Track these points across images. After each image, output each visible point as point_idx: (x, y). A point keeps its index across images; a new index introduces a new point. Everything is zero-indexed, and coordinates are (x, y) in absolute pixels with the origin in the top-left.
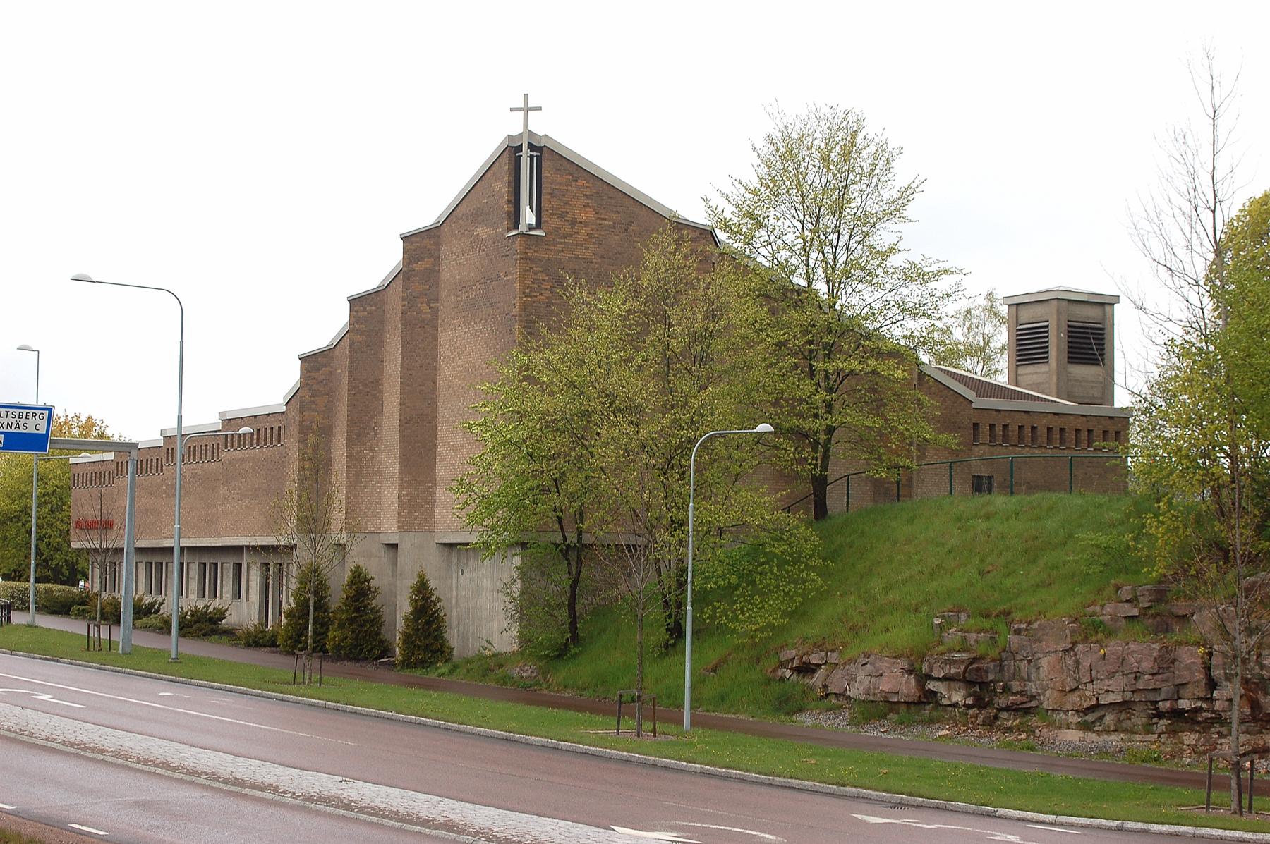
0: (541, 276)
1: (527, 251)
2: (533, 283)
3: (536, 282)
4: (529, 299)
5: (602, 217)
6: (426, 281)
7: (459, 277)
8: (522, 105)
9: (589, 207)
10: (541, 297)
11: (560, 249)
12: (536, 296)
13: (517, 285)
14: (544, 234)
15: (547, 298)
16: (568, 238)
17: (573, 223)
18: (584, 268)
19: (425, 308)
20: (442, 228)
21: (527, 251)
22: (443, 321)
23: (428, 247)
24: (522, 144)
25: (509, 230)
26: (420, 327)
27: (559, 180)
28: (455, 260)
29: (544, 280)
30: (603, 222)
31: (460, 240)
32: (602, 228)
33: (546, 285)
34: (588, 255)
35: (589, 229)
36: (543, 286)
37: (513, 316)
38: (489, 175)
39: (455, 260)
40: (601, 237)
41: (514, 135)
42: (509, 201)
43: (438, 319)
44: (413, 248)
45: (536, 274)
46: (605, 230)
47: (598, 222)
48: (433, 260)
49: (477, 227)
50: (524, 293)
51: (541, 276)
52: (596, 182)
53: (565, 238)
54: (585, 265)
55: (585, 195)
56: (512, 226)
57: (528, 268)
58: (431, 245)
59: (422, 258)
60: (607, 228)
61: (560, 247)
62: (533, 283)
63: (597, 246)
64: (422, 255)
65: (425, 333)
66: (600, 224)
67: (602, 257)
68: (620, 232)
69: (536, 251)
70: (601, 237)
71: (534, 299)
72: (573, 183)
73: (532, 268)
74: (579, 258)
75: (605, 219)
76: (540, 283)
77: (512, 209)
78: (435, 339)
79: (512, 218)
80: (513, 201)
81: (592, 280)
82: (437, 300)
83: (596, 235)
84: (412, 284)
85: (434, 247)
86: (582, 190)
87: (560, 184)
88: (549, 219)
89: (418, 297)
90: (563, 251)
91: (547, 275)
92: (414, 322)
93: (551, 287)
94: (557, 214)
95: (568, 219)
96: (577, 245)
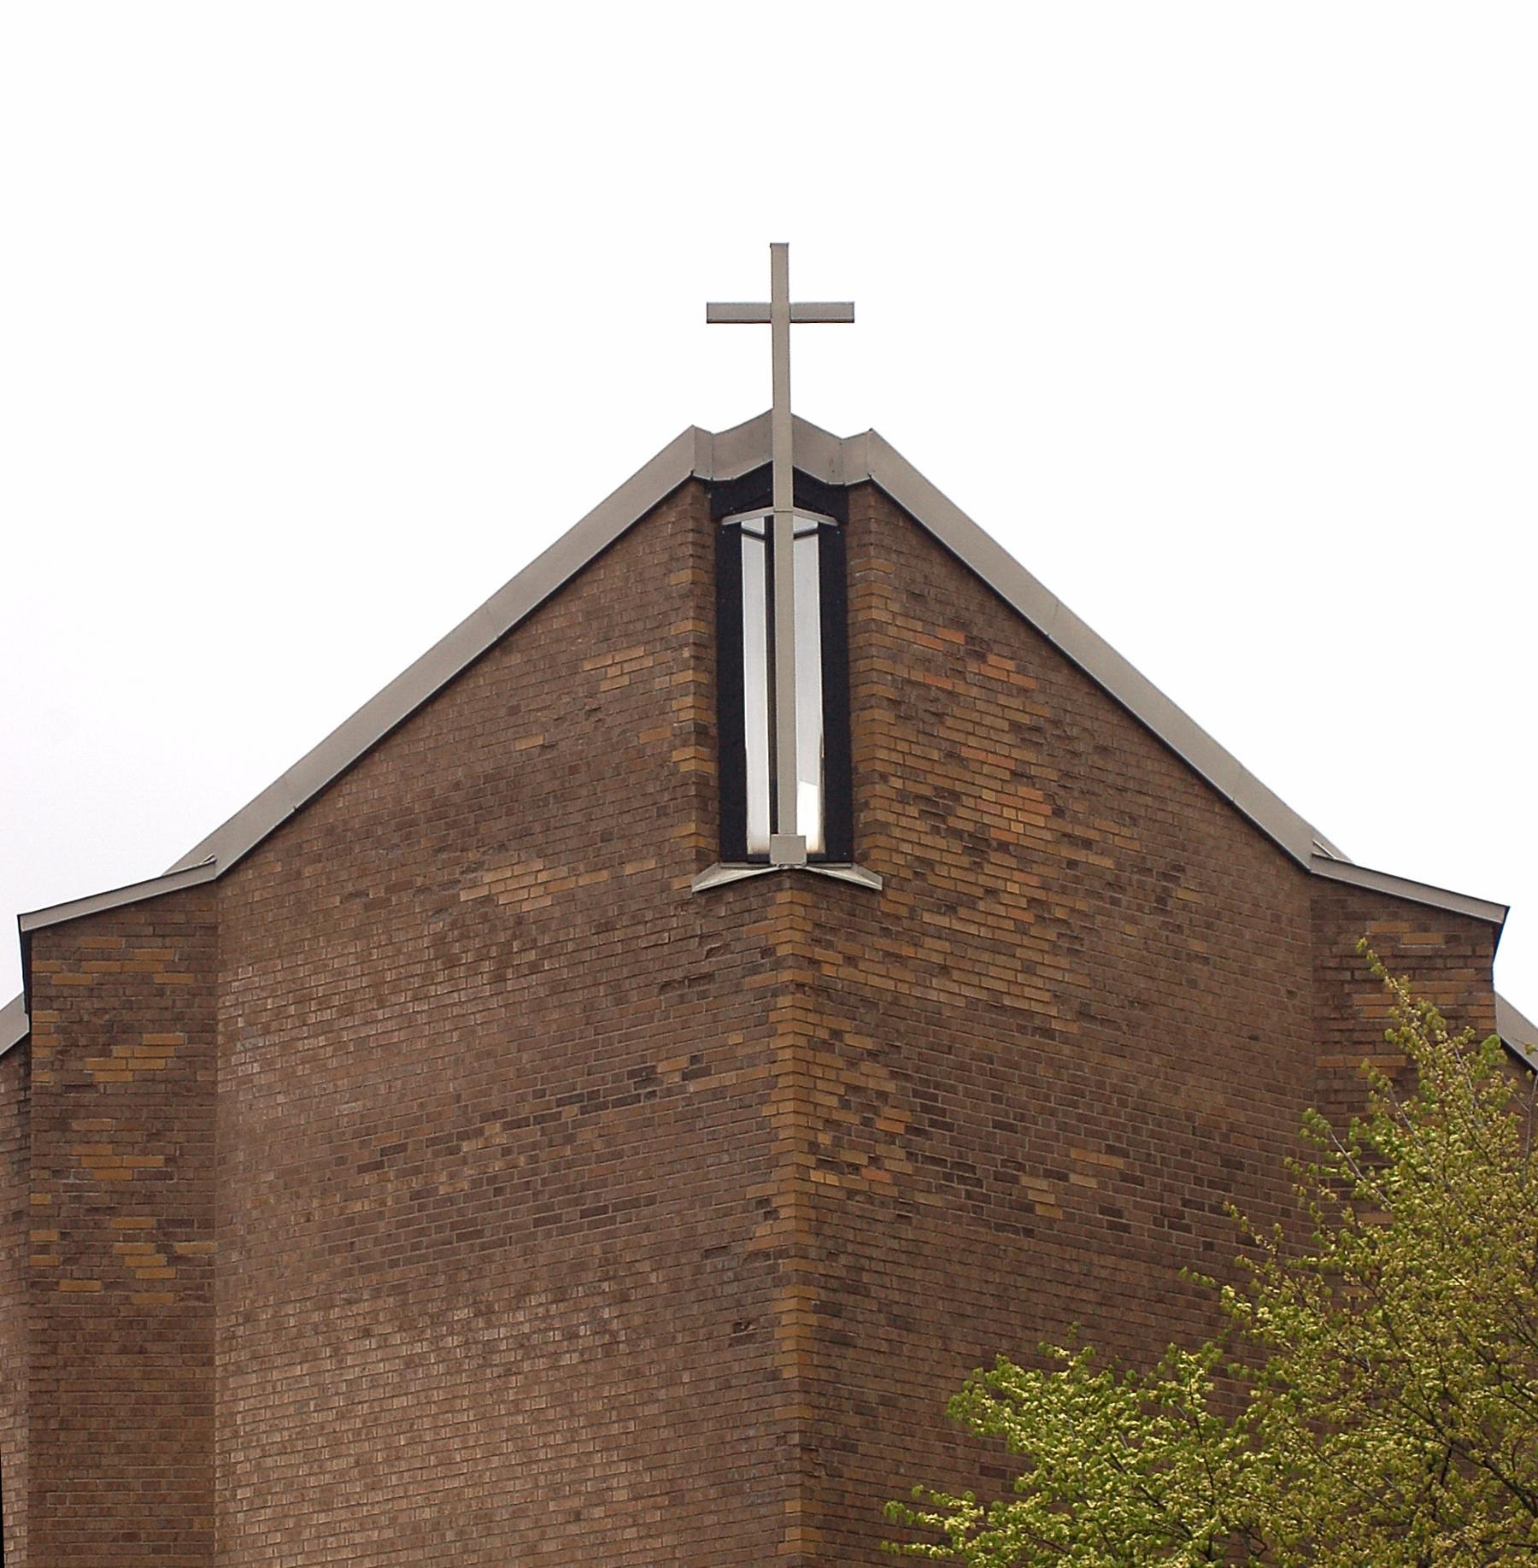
0: (875, 1077)
1: (819, 953)
2: (845, 1105)
3: (854, 1099)
4: (832, 1179)
5: (1079, 831)
6: (152, 1136)
7: (357, 1106)
8: (761, 294)
9: (1031, 780)
10: (871, 1173)
11: (937, 959)
12: (856, 1168)
13: (783, 1113)
14: (880, 887)
15: (898, 1178)
16: (963, 912)
17: (979, 845)
18: (1023, 1055)
19: (146, 1261)
20: (229, 891)
21: (819, 953)
22: (249, 1318)
23: (158, 979)
24: (769, 466)
25: (703, 862)
26: (123, 1351)
27: (923, 644)
28: (325, 1028)
29: (883, 1095)
30: (1081, 856)
31: (357, 935)
32: (1077, 880)
33: (890, 1120)
34: (1034, 997)
35: (1034, 881)
36: (881, 1124)
37: (754, 1255)
38: (557, 620)
39: (325, 1028)
40: (1076, 922)
41: (715, 430)
42: (701, 731)
43: (211, 1314)
44: (86, 980)
45: (852, 1064)
46: (1090, 893)
47: (1067, 852)
48: (180, 1036)
49: (479, 866)
50: (814, 1147)
51: (875, 1077)
52: (1052, 676)
53: (951, 909)
54: (1024, 1041)
55: (1016, 727)
56: (710, 844)
57: (823, 1034)
58: (171, 968)
59: (127, 1029)
60: (1097, 885)
61: (934, 950)
62: (845, 1105)
63: (1063, 962)
64: (127, 1016)
65: (146, 1377)
66: (1072, 864)
67: (1083, 1014)
68: (1140, 908)
69: (851, 960)
70: (1076, 922)
71: (852, 1180)
72: (973, 666)
73: (837, 1034)
74: (1003, 1009)
75: (1087, 844)
76: (870, 1103)
77: (711, 768)
78: (198, 1403)
79: (713, 806)
80: (713, 731)
81: (1053, 1113)
82: (208, 1224)
83: (1060, 913)
84: (80, 1149)
85: (186, 979)
86: (1002, 700)
87: (925, 662)
88: (892, 818)
89: (111, 1211)
90: (945, 970)
91: (894, 1075)
92: (90, 1325)
93: (910, 1129)
94: (918, 797)
95: (960, 825)
96: (996, 947)
